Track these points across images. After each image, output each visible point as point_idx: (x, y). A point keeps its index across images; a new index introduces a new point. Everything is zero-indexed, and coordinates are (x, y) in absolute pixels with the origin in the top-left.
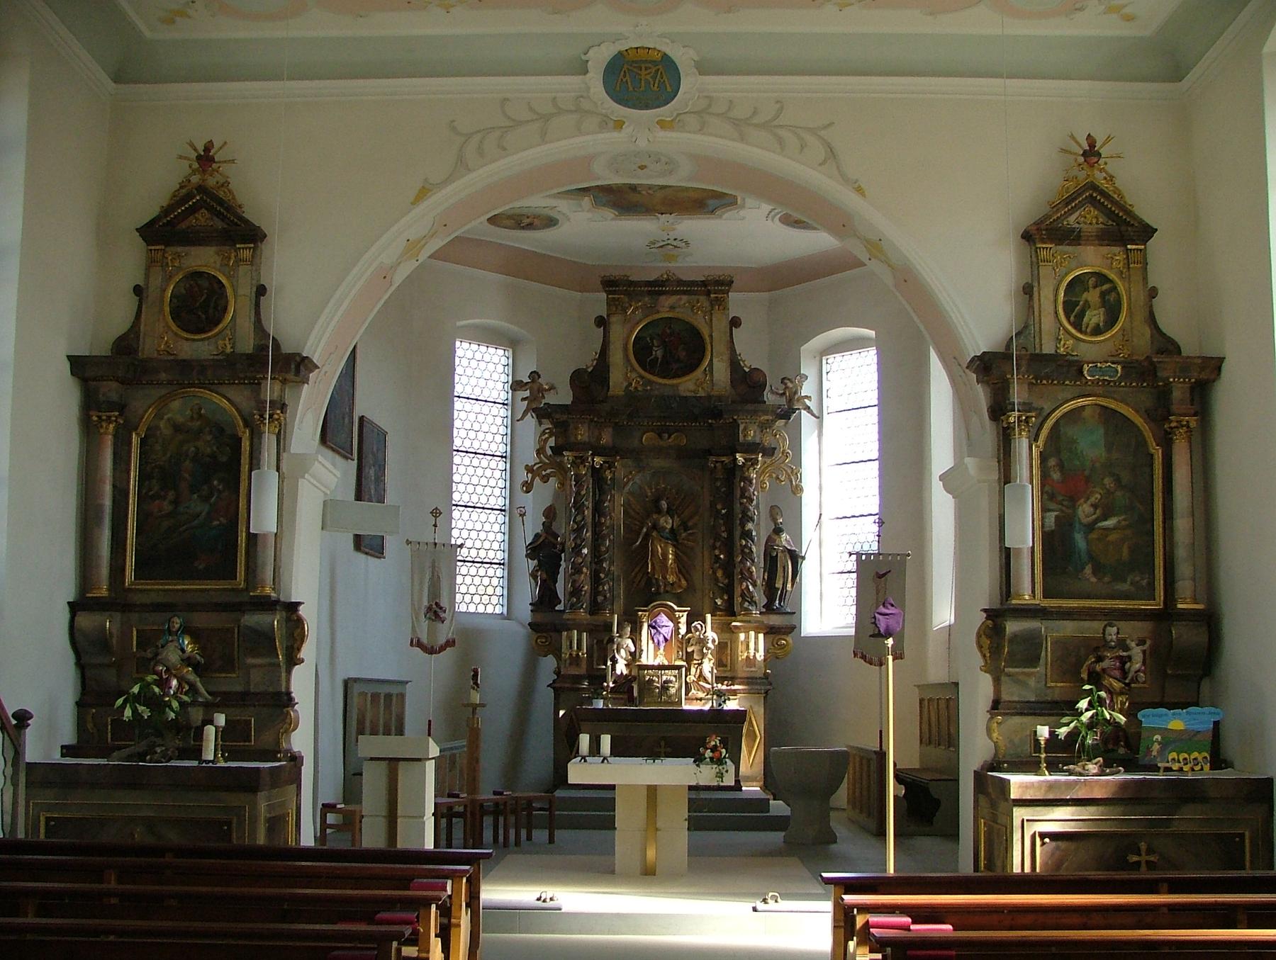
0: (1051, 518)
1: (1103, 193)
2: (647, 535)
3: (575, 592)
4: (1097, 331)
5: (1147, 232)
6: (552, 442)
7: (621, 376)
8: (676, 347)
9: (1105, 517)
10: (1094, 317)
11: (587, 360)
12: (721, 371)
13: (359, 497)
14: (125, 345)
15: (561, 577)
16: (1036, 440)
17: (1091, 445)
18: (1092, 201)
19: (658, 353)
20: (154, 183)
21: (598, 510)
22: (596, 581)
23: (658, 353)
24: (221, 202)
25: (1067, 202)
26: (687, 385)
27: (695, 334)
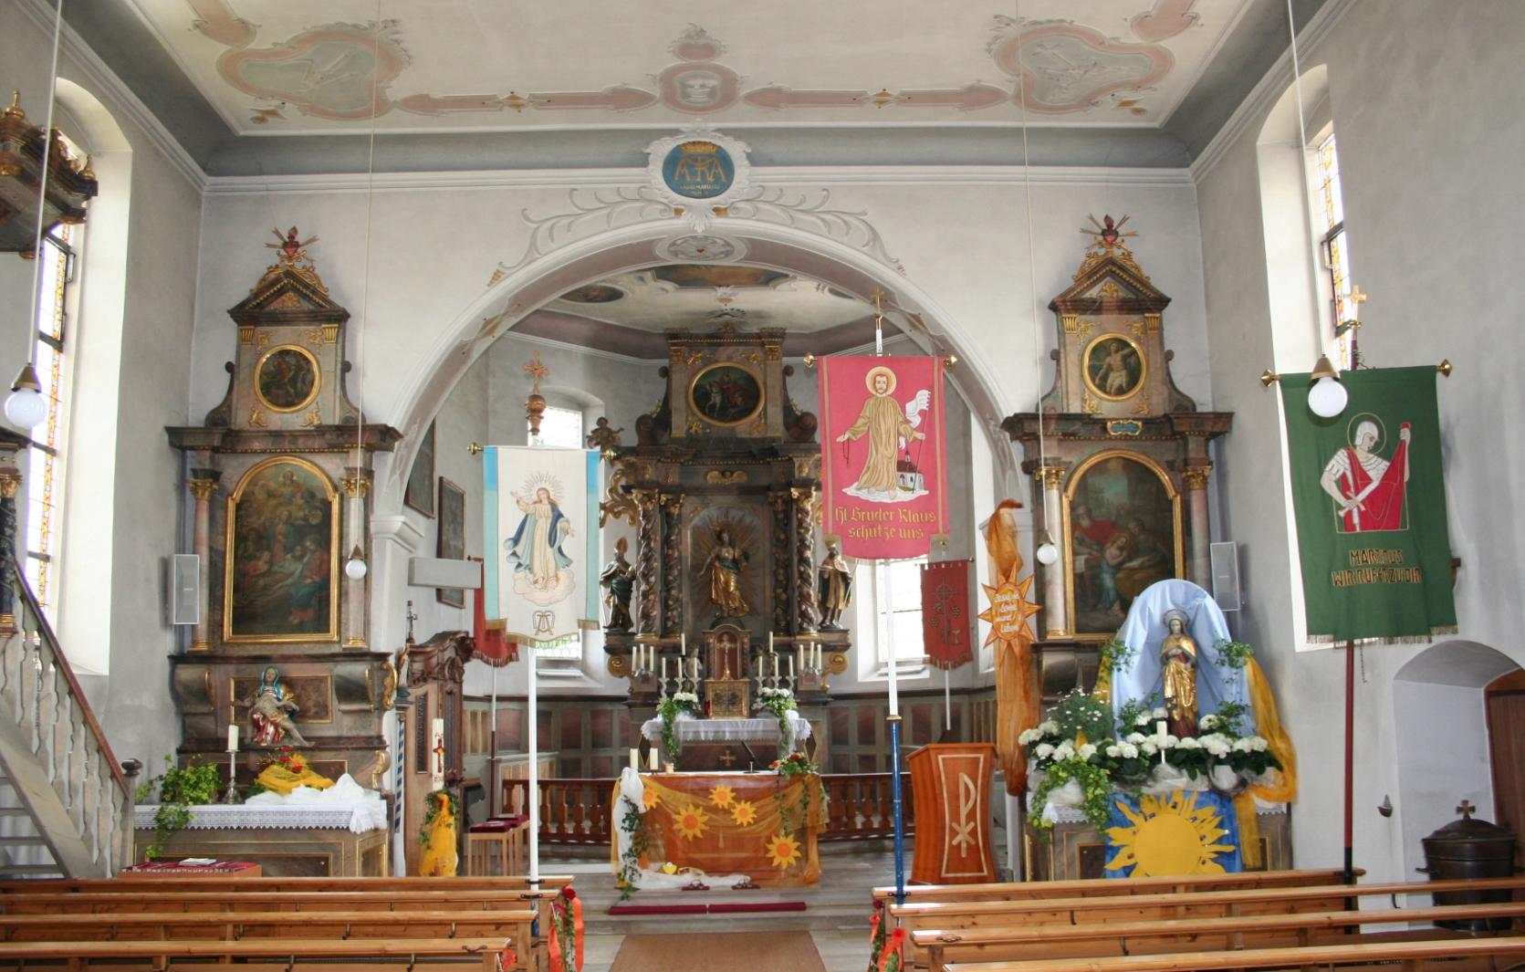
0: (1082, 559)
1: (1121, 268)
2: (711, 564)
3: (646, 615)
4: (1121, 391)
5: (1162, 302)
6: (623, 482)
7: (684, 423)
8: (737, 395)
9: (1130, 559)
10: (1117, 378)
11: (651, 408)
12: (776, 416)
13: (440, 554)
14: (218, 417)
15: (633, 604)
16: (1066, 489)
17: (1115, 491)
18: (1112, 274)
19: (717, 399)
20: (247, 268)
21: (667, 542)
22: (666, 607)
23: (717, 399)
24: (307, 286)
25: (1089, 276)
26: (744, 428)
27: (751, 381)
